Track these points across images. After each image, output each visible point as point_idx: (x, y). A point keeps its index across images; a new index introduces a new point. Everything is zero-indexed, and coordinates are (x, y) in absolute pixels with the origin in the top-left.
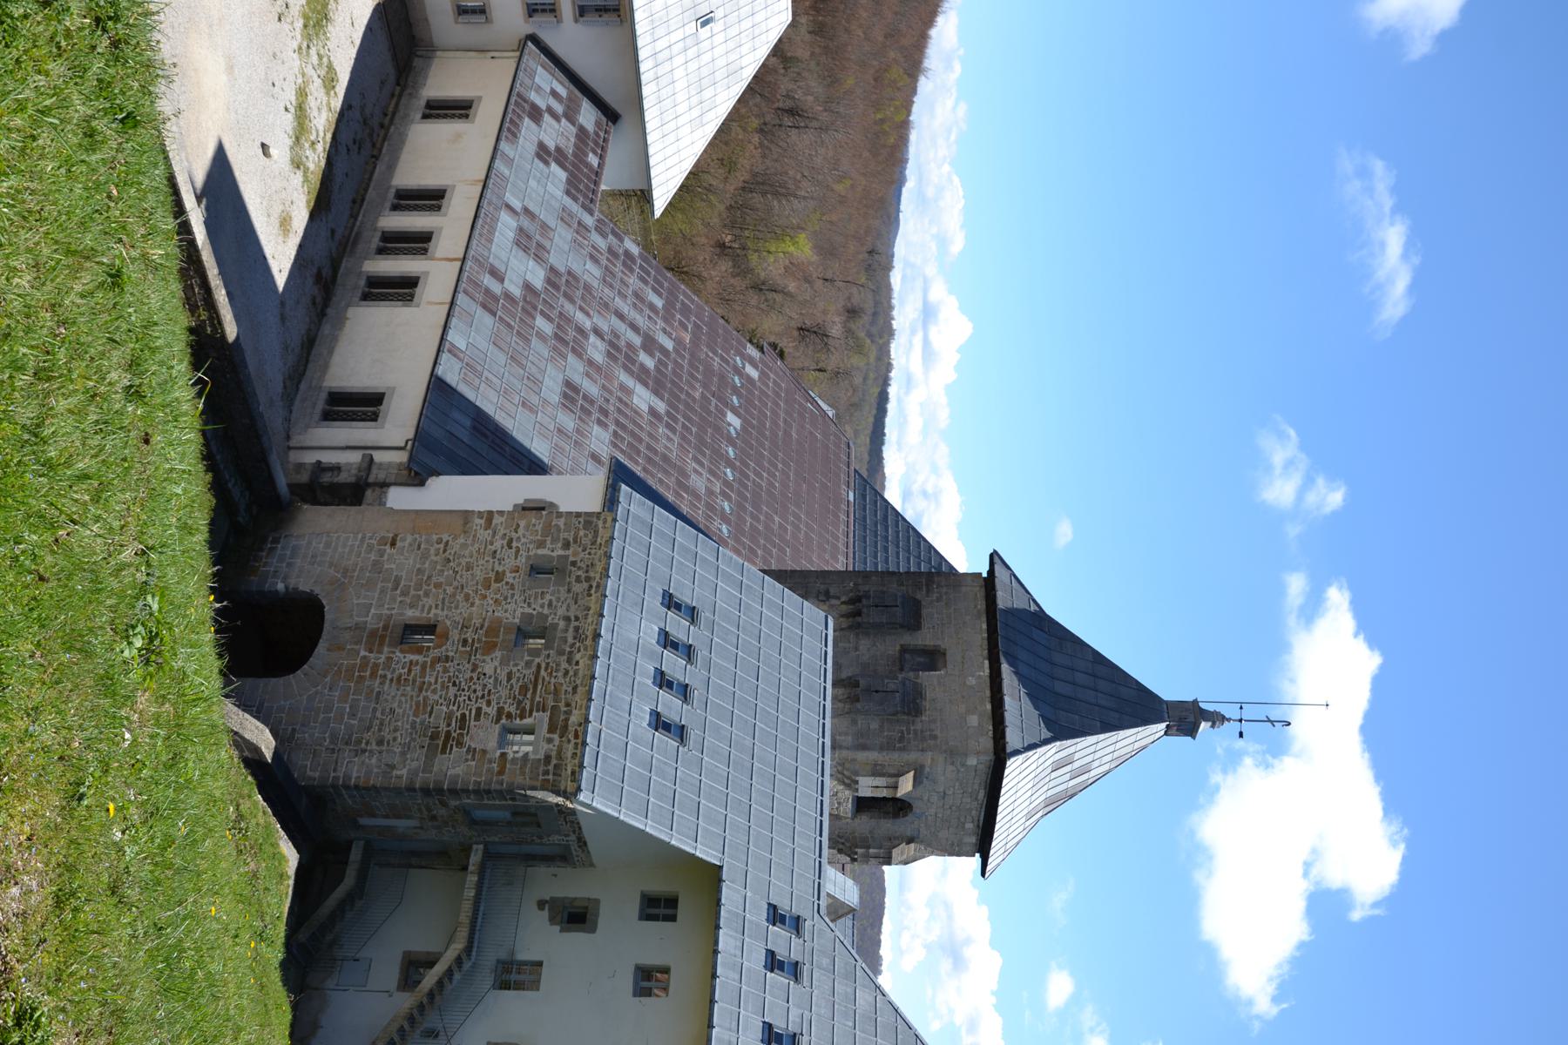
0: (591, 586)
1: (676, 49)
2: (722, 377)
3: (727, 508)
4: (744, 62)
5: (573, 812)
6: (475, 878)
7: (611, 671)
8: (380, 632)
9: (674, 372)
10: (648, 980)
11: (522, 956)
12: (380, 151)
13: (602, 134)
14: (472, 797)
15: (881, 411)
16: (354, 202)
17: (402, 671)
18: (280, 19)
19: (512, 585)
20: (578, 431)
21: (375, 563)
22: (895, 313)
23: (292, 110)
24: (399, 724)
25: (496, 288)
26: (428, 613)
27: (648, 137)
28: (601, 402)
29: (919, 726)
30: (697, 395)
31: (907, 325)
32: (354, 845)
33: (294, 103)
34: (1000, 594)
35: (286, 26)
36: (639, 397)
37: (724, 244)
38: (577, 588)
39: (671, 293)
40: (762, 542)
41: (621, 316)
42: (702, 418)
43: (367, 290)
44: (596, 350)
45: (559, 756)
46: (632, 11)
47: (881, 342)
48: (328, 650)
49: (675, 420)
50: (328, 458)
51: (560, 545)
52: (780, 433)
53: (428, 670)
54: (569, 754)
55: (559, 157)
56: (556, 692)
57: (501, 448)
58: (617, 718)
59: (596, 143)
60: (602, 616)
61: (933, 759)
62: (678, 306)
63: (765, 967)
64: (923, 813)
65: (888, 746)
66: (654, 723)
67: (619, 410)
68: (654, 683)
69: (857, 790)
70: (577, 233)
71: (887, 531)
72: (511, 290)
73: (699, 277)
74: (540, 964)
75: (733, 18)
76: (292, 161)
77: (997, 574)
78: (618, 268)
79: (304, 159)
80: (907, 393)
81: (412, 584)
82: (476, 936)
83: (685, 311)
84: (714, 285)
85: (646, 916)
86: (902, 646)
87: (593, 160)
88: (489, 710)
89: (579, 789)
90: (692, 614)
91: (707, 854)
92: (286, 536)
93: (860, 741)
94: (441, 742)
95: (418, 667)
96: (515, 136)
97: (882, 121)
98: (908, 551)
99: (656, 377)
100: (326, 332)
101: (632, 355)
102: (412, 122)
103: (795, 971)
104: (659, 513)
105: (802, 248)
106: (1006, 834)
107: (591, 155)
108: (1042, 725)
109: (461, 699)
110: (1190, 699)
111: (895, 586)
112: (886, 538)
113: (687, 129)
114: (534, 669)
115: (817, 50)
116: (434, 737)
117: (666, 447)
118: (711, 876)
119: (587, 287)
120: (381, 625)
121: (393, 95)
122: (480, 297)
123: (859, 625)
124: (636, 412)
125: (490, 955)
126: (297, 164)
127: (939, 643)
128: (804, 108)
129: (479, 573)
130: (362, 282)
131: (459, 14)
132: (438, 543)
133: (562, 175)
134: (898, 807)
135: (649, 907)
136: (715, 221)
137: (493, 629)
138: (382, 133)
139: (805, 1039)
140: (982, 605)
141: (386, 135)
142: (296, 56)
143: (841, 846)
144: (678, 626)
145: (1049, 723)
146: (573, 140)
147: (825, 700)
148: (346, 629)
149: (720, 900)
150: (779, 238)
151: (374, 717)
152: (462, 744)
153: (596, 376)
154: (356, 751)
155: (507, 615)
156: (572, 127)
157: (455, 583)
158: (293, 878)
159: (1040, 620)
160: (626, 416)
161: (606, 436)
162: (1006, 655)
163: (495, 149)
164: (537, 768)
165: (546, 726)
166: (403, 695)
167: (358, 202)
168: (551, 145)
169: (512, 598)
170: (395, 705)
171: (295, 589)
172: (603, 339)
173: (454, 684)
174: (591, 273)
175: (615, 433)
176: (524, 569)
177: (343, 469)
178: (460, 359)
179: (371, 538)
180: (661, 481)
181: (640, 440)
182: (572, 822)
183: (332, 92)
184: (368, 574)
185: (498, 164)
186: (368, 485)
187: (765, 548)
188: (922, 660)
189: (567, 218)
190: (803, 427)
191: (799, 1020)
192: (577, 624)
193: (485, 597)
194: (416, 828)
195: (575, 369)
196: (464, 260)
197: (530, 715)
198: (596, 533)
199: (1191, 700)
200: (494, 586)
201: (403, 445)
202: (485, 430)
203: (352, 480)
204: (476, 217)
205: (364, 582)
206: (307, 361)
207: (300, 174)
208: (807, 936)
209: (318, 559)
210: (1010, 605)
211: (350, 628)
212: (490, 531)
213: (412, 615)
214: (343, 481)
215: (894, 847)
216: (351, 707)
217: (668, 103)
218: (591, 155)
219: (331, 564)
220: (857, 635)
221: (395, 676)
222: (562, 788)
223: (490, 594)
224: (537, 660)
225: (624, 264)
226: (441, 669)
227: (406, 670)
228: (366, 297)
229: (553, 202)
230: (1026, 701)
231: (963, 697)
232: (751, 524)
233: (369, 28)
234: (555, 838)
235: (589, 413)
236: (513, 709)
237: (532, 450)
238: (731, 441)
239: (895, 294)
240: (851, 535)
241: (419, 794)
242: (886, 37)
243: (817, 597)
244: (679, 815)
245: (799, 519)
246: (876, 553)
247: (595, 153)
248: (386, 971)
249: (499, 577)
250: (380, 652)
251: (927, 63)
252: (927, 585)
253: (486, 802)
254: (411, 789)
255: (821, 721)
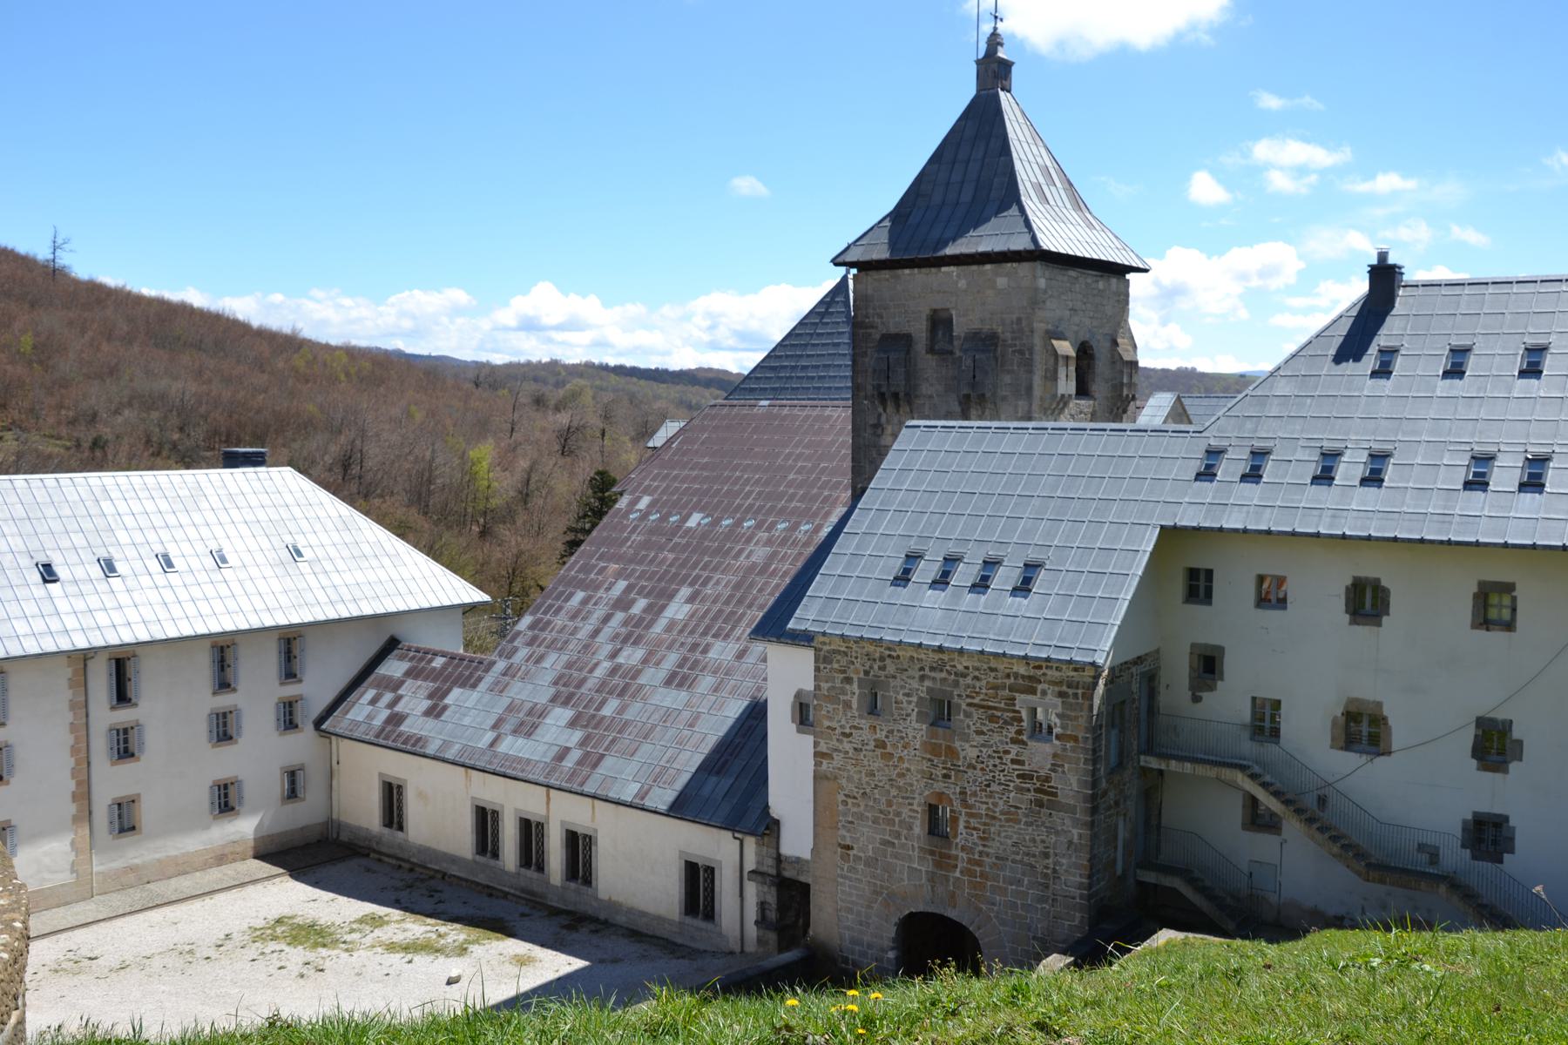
0: (889, 656)
1: (325, 582)
2: (651, 532)
3: (783, 526)
4: (334, 514)
5: (1112, 669)
6: (1173, 763)
7: (974, 635)
8: (937, 858)
9: (650, 579)
10: (1270, 596)
11: (1246, 715)
12: (437, 871)
13: (412, 654)
14: (1098, 766)
15: (634, 372)
16: (490, 895)
17: (975, 835)
18: (322, 970)
19: (888, 732)
20: (715, 672)
21: (867, 864)
22: (534, 359)
23: (409, 956)
24: (1027, 838)
25: (576, 755)
26: (917, 812)
27: (412, 608)
28: (684, 651)
29: (1008, 335)
30: (671, 556)
31: (544, 347)
32: (1141, 879)
33: (402, 955)
34: (875, 256)
35: (327, 964)
36: (676, 612)
37: (481, 532)
38: (891, 669)
39: (569, 584)
40: (815, 490)
41: (596, 632)
42: (694, 551)
43: (580, 881)
44: (631, 656)
45: (1060, 683)
46: (291, 626)
47: (564, 374)
48: (954, 907)
49: (698, 577)
50: (752, 913)
51: (848, 687)
52: (705, 474)
53: (973, 811)
54: (1057, 674)
55: (438, 695)
56: (996, 688)
57: (737, 746)
58: (1021, 629)
59: (422, 659)
60: (920, 645)
61: (1041, 321)
62: (581, 576)
63: (1257, 483)
64: (1090, 331)
65: (1028, 365)
66: (1024, 593)
67: (692, 632)
68: (984, 594)
69: (1070, 396)
70: (514, 676)
71: (786, 367)
72: (577, 740)
73: (518, 556)
74: (1254, 699)
75: (292, 526)
76: (460, 955)
77: (854, 259)
78: (548, 636)
79: (456, 944)
80: (612, 346)
81: (888, 828)
82: (1229, 761)
83: (586, 569)
84: (526, 541)
85: (1208, 598)
86: (927, 353)
87: (438, 662)
88: (1014, 752)
89: (1093, 664)
90: (913, 558)
91: (1149, 541)
92: (841, 951)
93: (1023, 393)
94: (1045, 797)
95: (972, 820)
96: (419, 739)
97: (347, 374)
98: (806, 345)
99: (656, 597)
100: (624, 919)
101: (635, 621)
102: (406, 841)
103: (1259, 455)
104: (814, 591)
105: (484, 453)
106: (1109, 249)
107: (434, 664)
108: (1005, 214)
109: (1003, 779)
110: (974, 67)
111: (867, 360)
112: (794, 368)
113: (402, 569)
114: (972, 709)
115: (280, 441)
116: (1040, 804)
117: (726, 586)
118: (1169, 535)
119: (569, 665)
120: (930, 857)
121: (380, 860)
122: (586, 770)
123: (907, 394)
124: (692, 616)
125: (1247, 747)
126: (462, 951)
127: (924, 317)
128: (342, 453)
129: (876, 765)
130: (573, 885)
131: (296, 796)
132: (847, 804)
133: (456, 692)
134: (1085, 353)
135: (1198, 596)
136: (463, 541)
137: (934, 750)
138: (418, 870)
139: (1326, 444)
140: (886, 274)
141: (420, 866)
142: (355, 954)
143: (1120, 411)
144: (926, 571)
145: (1003, 207)
146: (419, 683)
147: (990, 428)
148: (933, 891)
149: (1194, 528)
150: (474, 477)
151: (1021, 862)
152: (1047, 777)
153: (658, 656)
154: (1054, 878)
155: (919, 735)
156: (407, 684)
157: (887, 787)
158: (1186, 934)
159: (900, 216)
160: (697, 625)
161: (718, 645)
162: (936, 249)
163: (434, 758)
164: (1071, 705)
165: (1030, 697)
166: (999, 835)
167: (490, 892)
168: (426, 704)
169: (901, 732)
170: (1009, 842)
171: (894, 940)
172: (620, 649)
173: (988, 786)
174: (554, 663)
175: (714, 636)
176: (872, 721)
177: (762, 899)
178: (650, 788)
179: (843, 869)
180: (760, 590)
181: (720, 611)
182: (1121, 670)
183: (386, 919)
184: (879, 871)
185: (449, 755)
186: (779, 875)
187: (821, 488)
188: (940, 333)
189: (500, 687)
190: (697, 452)
191: (1308, 451)
192: (927, 669)
193: (901, 758)
194: (1125, 820)
195: (652, 677)
196: (548, 786)
197: (1019, 712)
198: (835, 652)
199: (975, 66)
200: (889, 749)
201: (738, 842)
202: (720, 763)
203: (774, 890)
204: (505, 776)
205: (887, 874)
206: (652, 937)
207: (472, 948)
208: (1225, 443)
209: (864, 919)
210: (886, 247)
211: (933, 887)
212: (835, 754)
213: (919, 829)
214: (775, 898)
215: (1122, 358)
216: (1012, 885)
217: (379, 590)
218: (434, 664)
219: (869, 907)
220: (916, 396)
221: (980, 842)
222: (1091, 680)
223: (898, 753)
224: (964, 706)
225: (542, 630)
226: (973, 799)
227: (974, 832)
228: (588, 881)
229: (485, 700)
230: (981, 230)
231: (979, 292)
232: (798, 501)
233: (316, 884)
234: (1135, 687)
235: (696, 662)
236: (1013, 729)
237: (736, 716)
238: (716, 523)
239: (515, 359)
240: (804, 402)
241: (1096, 817)
242: (263, 372)
243: (879, 436)
244: (1113, 569)
245: (790, 454)
246: (808, 378)
247: (431, 661)
248: (1261, 846)
249: (881, 744)
250: (956, 858)
251: (287, 330)
252: (866, 328)
253: (1103, 753)
254: (1092, 825)
255: (1049, 431)
